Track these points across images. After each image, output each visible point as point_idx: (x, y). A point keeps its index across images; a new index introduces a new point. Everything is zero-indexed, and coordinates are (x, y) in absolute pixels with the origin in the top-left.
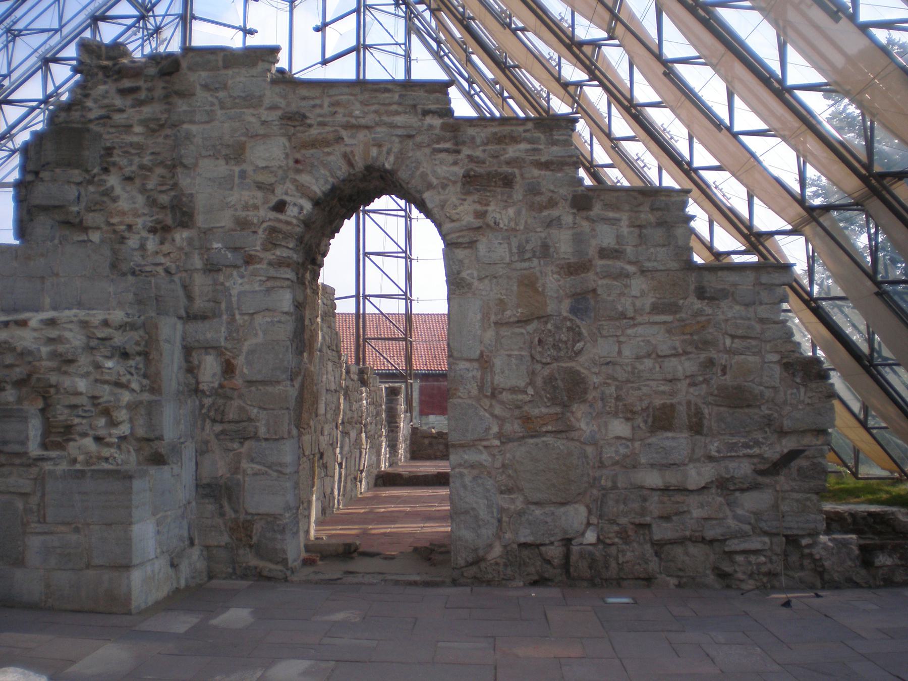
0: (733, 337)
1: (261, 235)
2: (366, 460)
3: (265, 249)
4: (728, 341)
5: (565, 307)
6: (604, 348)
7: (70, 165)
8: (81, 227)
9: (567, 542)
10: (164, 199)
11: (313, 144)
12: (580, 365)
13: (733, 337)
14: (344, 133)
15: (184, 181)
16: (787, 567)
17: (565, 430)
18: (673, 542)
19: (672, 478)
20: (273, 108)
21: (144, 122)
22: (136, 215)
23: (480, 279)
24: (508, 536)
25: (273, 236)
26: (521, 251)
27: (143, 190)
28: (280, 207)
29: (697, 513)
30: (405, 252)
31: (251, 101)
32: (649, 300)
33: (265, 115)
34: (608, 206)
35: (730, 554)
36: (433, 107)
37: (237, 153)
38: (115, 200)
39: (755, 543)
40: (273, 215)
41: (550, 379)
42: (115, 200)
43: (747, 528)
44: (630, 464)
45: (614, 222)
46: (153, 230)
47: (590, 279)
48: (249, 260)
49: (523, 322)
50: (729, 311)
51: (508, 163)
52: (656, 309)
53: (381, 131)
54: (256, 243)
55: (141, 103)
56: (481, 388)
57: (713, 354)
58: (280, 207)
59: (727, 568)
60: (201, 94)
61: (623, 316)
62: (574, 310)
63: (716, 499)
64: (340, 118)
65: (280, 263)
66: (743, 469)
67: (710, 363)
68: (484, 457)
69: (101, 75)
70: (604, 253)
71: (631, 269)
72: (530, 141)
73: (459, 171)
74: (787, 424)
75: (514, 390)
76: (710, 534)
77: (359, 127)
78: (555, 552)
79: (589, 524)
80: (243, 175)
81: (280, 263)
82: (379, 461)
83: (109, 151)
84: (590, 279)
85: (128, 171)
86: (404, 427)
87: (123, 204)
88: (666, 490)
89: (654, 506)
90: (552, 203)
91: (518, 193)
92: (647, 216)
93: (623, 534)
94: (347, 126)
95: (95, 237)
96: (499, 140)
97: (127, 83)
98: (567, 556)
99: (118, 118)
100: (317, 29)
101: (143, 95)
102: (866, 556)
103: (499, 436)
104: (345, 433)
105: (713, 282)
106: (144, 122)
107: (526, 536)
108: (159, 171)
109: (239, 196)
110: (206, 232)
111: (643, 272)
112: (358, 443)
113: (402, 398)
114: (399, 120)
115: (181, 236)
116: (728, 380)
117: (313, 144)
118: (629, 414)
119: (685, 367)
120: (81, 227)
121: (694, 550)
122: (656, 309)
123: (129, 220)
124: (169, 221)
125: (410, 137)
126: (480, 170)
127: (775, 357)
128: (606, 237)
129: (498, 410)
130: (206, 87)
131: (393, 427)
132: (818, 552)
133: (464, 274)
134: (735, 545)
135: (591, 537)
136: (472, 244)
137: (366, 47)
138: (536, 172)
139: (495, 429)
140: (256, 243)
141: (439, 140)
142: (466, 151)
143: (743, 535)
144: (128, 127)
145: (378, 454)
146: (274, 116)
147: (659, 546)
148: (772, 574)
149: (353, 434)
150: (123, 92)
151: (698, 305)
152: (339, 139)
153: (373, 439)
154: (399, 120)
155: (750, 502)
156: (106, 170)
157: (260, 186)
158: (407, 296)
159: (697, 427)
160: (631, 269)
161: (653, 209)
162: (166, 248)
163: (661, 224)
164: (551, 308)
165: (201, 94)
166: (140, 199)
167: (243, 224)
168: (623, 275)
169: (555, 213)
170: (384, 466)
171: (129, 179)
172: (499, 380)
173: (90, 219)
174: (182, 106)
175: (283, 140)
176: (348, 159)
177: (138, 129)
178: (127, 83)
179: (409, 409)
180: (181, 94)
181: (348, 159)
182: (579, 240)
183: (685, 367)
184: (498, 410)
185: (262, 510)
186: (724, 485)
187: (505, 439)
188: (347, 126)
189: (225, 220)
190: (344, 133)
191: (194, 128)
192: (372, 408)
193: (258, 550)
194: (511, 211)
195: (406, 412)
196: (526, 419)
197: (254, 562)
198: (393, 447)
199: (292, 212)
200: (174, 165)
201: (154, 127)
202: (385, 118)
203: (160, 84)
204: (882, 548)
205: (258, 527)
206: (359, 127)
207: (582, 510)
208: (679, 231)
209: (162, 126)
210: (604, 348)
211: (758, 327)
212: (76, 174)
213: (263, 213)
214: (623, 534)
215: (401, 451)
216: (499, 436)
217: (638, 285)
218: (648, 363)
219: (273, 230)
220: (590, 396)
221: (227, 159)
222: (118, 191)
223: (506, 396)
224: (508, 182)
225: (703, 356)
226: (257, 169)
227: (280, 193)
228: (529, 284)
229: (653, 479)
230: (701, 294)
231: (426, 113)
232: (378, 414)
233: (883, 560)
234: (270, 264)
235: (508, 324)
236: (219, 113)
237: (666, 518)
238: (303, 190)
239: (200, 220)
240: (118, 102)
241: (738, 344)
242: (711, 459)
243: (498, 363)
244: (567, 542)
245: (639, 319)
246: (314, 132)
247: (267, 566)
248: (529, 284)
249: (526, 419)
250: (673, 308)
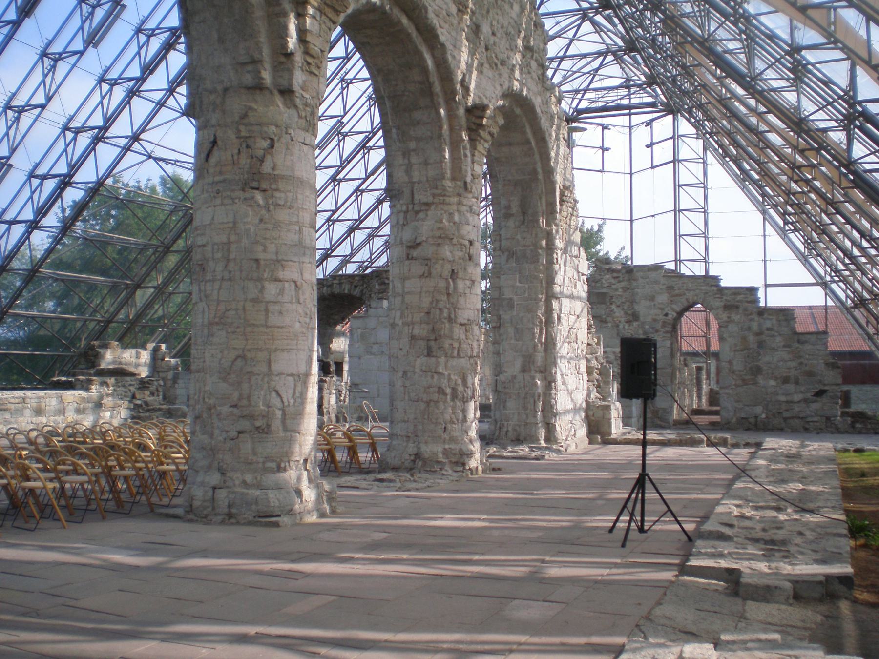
0: (809, 355)
1: (661, 324)
2: (687, 402)
3: (662, 328)
4: (807, 356)
5: (755, 346)
6: (767, 358)
7: (602, 303)
8: (606, 322)
9: (756, 417)
10: (630, 312)
11: (677, 295)
12: (759, 363)
13: (809, 355)
14: (686, 292)
15: (636, 307)
16: (827, 427)
17: (755, 383)
18: (790, 418)
19: (789, 398)
20: (664, 284)
21: (622, 288)
22: (621, 317)
23: (729, 337)
24: (738, 415)
25: (664, 324)
26: (742, 329)
27: (623, 309)
28: (666, 315)
29: (797, 409)
30: (704, 184)
31: (657, 282)
32: (782, 344)
33: (662, 287)
34: (769, 315)
35: (808, 422)
36: (713, 284)
37: (652, 299)
38: (615, 313)
39: (815, 419)
40: (664, 317)
41: (751, 368)
42: (615, 313)
43: (813, 414)
44: (776, 394)
45: (771, 319)
46: (627, 322)
47: (763, 337)
48: (657, 331)
49: (742, 350)
50: (808, 347)
51: (738, 301)
52: (784, 346)
53: (697, 291)
54: (659, 326)
55: (620, 282)
56: (729, 370)
57: (802, 360)
58: (666, 315)
59: (807, 426)
60: (641, 280)
61: (773, 348)
62: (759, 347)
63: (803, 405)
64: (685, 288)
65: (667, 332)
66: (809, 395)
67: (801, 363)
68: (730, 391)
69: (606, 272)
70: (768, 329)
71: (776, 334)
72: (744, 294)
73: (722, 304)
74: (826, 382)
75: (740, 371)
76: (801, 416)
77: (690, 290)
78: (752, 420)
79: (763, 412)
80: (654, 305)
81: (667, 332)
82: (692, 403)
83: (612, 297)
84: (763, 337)
85: (618, 303)
86: (705, 388)
87: (617, 314)
88: (787, 402)
89: (784, 407)
90: (751, 314)
91: (741, 311)
92: (781, 318)
93: (774, 415)
94: (687, 290)
95: (610, 325)
96: (735, 294)
97: (615, 275)
98: (756, 421)
99: (614, 286)
100: (648, 146)
101: (621, 279)
102: (852, 425)
103: (735, 385)
104: (679, 388)
105: (802, 338)
106: (622, 288)
107: (743, 415)
108: (627, 303)
109: (654, 312)
110: (643, 323)
111: (780, 335)
112: (683, 393)
113: (704, 372)
114: (703, 288)
115: (635, 324)
116: (807, 368)
117: (677, 295)
118: (776, 379)
119: (793, 364)
120: (606, 322)
121: (796, 421)
122: (784, 346)
123: (619, 319)
124: (631, 319)
125: (707, 293)
126: (729, 303)
127: (822, 361)
128: (768, 324)
129: (735, 377)
130: (642, 278)
131: (699, 388)
132: (836, 422)
133: (724, 336)
134: (809, 419)
135: (764, 416)
136: (726, 326)
137: (679, 161)
138: (747, 304)
139: (734, 383)
140: (659, 326)
141: (716, 294)
142: (725, 298)
143: (812, 416)
144: (616, 290)
145: (692, 400)
146: (664, 287)
147: (785, 419)
148: (821, 429)
149: (682, 389)
150: (614, 278)
151: (798, 345)
152: (684, 294)
153: (690, 391)
154: (703, 288)
155: (814, 406)
156: (611, 304)
157: (660, 309)
158: (705, 260)
159: (797, 383)
160: (776, 334)
161: (784, 315)
162: (631, 327)
163: (786, 320)
164: (751, 346)
165: (641, 280)
166: (622, 313)
167: (655, 320)
168: (773, 336)
169: (752, 317)
170: (695, 406)
171: (618, 306)
172: (735, 368)
173: (609, 319)
174: (634, 284)
175: (666, 295)
176: (687, 300)
177: (620, 290)
178: (615, 275)
179: (708, 378)
180: (634, 280)
181: (687, 300)
182: (760, 325)
183: (793, 364)
184: (735, 377)
185: (663, 407)
186: (805, 401)
187: (737, 386)
188: (687, 290)
189: (649, 319)
190: (686, 292)
191: (639, 291)
192: (690, 377)
193: (660, 419)
194: (739, 316)
195: (707, 379)
196: (744, 380)
197: (659, 423)
198: (699, 397)
199: (670, 316)
200: (633, 302)
201: (625, 289)
202: (699, 288)
203: (627, 275)
204: (858, 422)
205: (661, 412)
206: (690, 290)
207: (761, 408)
208: (792, 322)
209: (628, 289)
210: (767, 358)
211: (817, 352)
212: (603, 306)
213: (661, 317)
214: (774, 415)
215: (704, 401)
216: (735, 385)
217: (778, 339)
218: (782, 363)
219: (664, 322)
220: (764, 373)
221: (650, 300)
222: (615, 310)
223: (737, 373)
224: (737, 307)
225: (799, 361)
226: (659, 303)
227: (666, 311)
228: (744, 339)
229: (783, 398)
230: (799, 341)
231: (712, 286)
232: (692, 380)
233: (858, 425)
234: (664, 332)
235: (738, 351)
236: (647, 286)
237: (787, 410)
238: (673, 310)
239: (641, 319)
240: (613, 281)
241: (811, 357)
242: (802, 392)
243: (735, 363)
244: (756, 417)
245: (780, 349)
246: (677, 292)
247: (663, 424)
248: (744, 339)
249: (744, 380)
250: (788, 346)
